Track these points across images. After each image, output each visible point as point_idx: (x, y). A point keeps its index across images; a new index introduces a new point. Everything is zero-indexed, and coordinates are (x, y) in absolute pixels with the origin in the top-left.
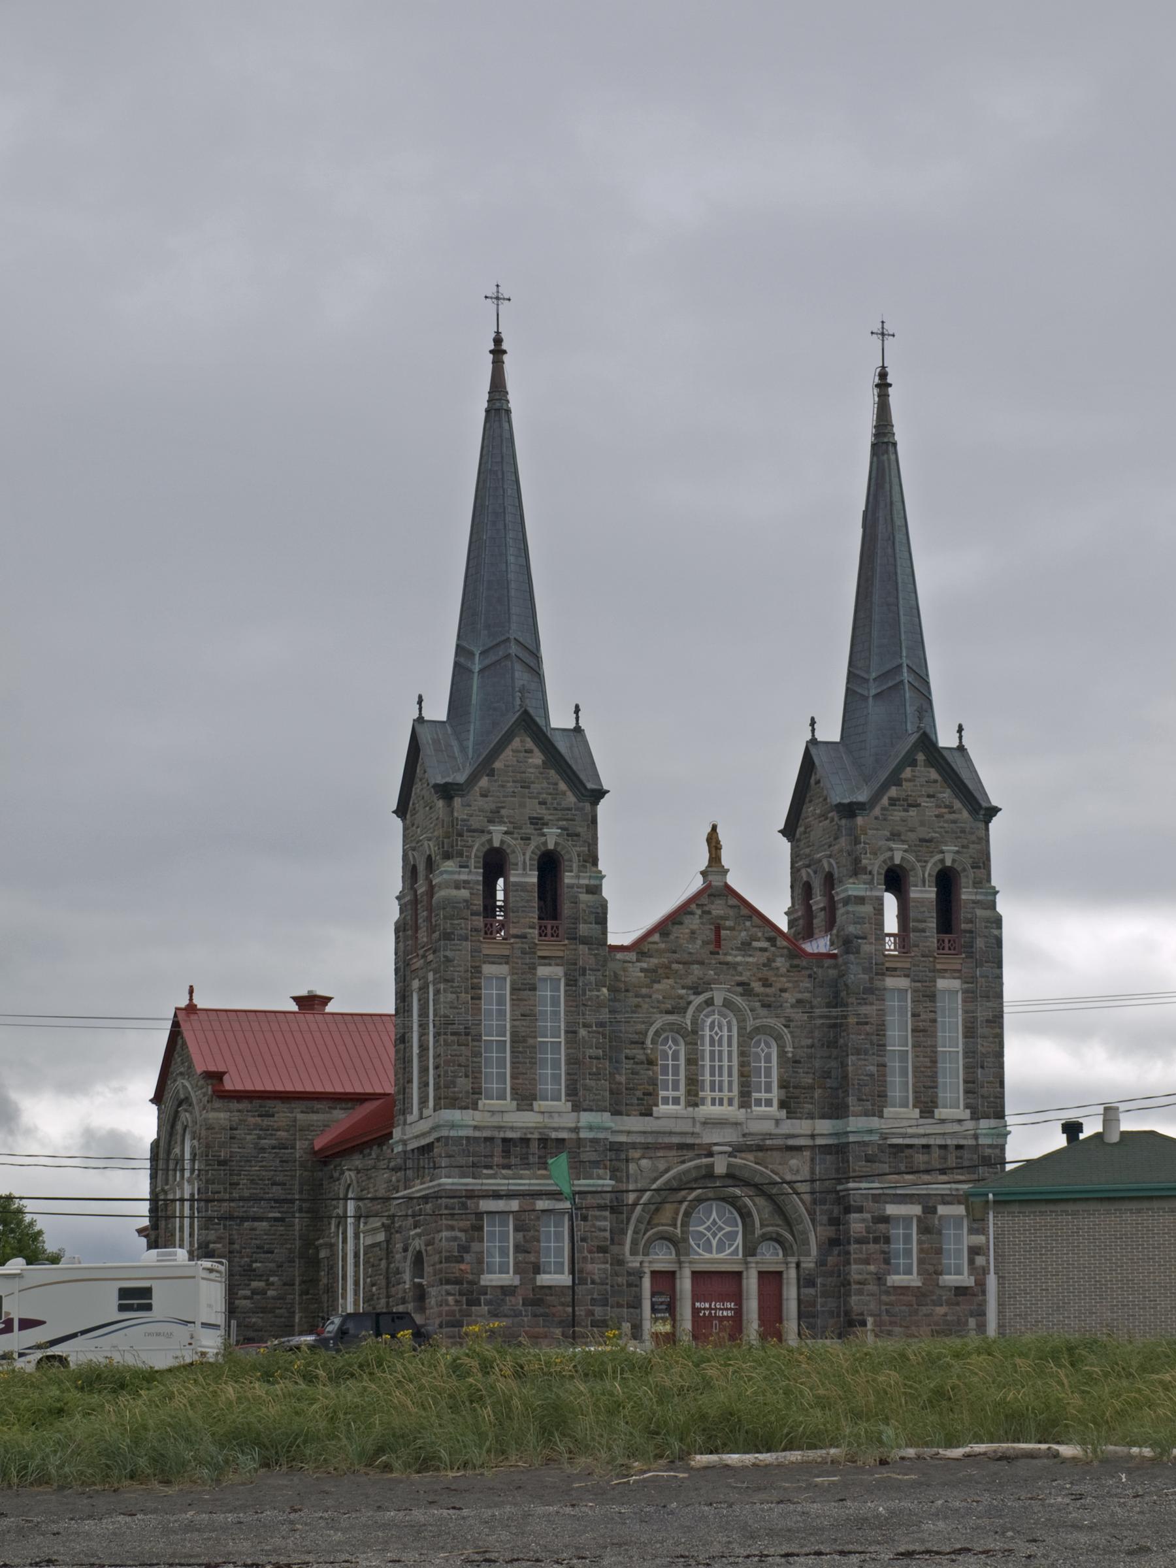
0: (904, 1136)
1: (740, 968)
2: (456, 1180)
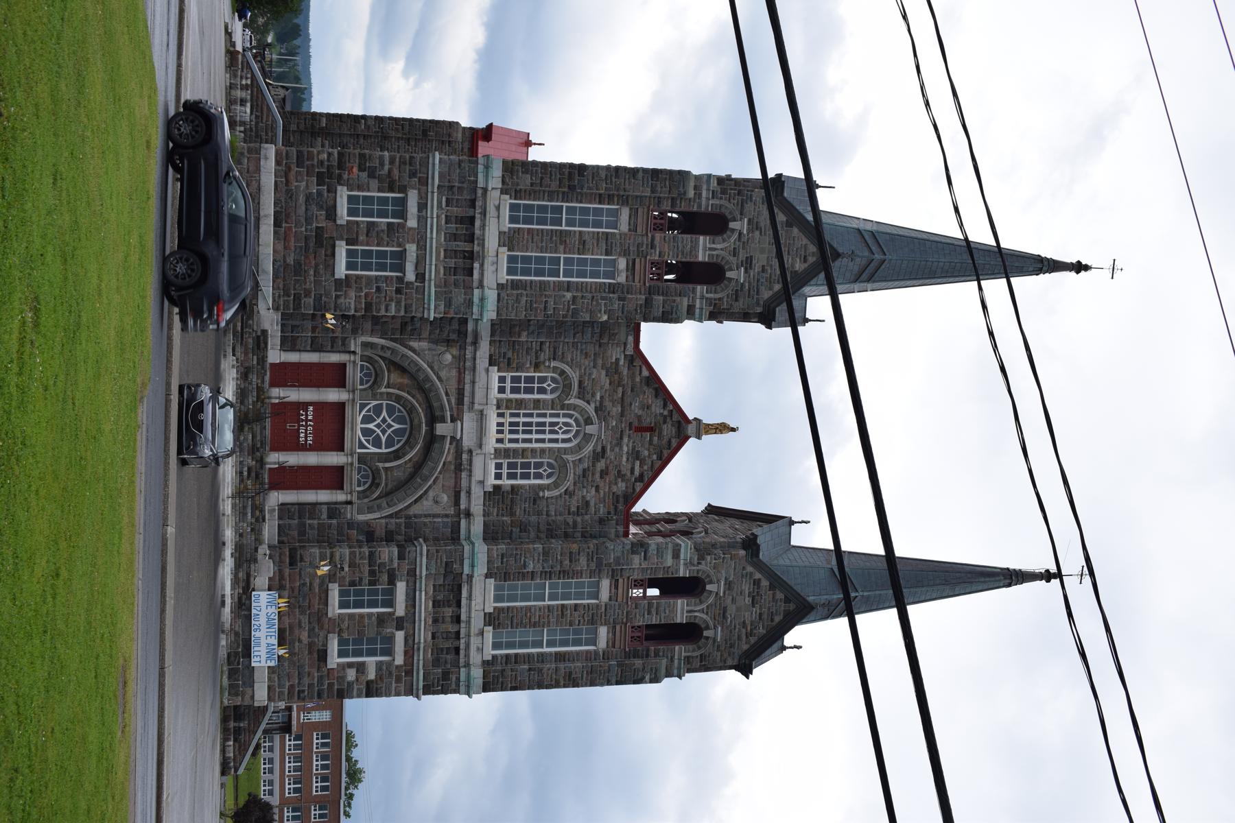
0: (470, 598)
1: (617, 449)
2: (437, 167)
